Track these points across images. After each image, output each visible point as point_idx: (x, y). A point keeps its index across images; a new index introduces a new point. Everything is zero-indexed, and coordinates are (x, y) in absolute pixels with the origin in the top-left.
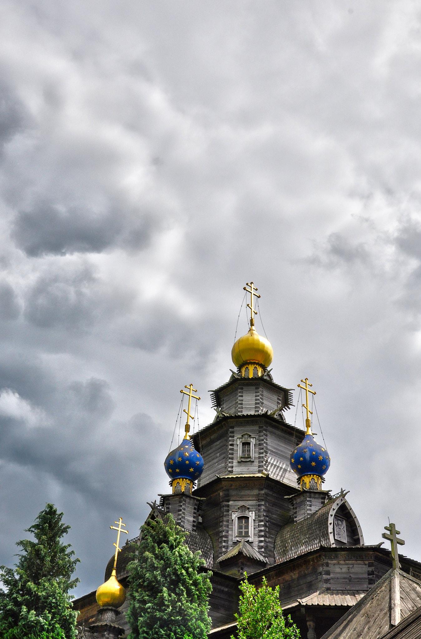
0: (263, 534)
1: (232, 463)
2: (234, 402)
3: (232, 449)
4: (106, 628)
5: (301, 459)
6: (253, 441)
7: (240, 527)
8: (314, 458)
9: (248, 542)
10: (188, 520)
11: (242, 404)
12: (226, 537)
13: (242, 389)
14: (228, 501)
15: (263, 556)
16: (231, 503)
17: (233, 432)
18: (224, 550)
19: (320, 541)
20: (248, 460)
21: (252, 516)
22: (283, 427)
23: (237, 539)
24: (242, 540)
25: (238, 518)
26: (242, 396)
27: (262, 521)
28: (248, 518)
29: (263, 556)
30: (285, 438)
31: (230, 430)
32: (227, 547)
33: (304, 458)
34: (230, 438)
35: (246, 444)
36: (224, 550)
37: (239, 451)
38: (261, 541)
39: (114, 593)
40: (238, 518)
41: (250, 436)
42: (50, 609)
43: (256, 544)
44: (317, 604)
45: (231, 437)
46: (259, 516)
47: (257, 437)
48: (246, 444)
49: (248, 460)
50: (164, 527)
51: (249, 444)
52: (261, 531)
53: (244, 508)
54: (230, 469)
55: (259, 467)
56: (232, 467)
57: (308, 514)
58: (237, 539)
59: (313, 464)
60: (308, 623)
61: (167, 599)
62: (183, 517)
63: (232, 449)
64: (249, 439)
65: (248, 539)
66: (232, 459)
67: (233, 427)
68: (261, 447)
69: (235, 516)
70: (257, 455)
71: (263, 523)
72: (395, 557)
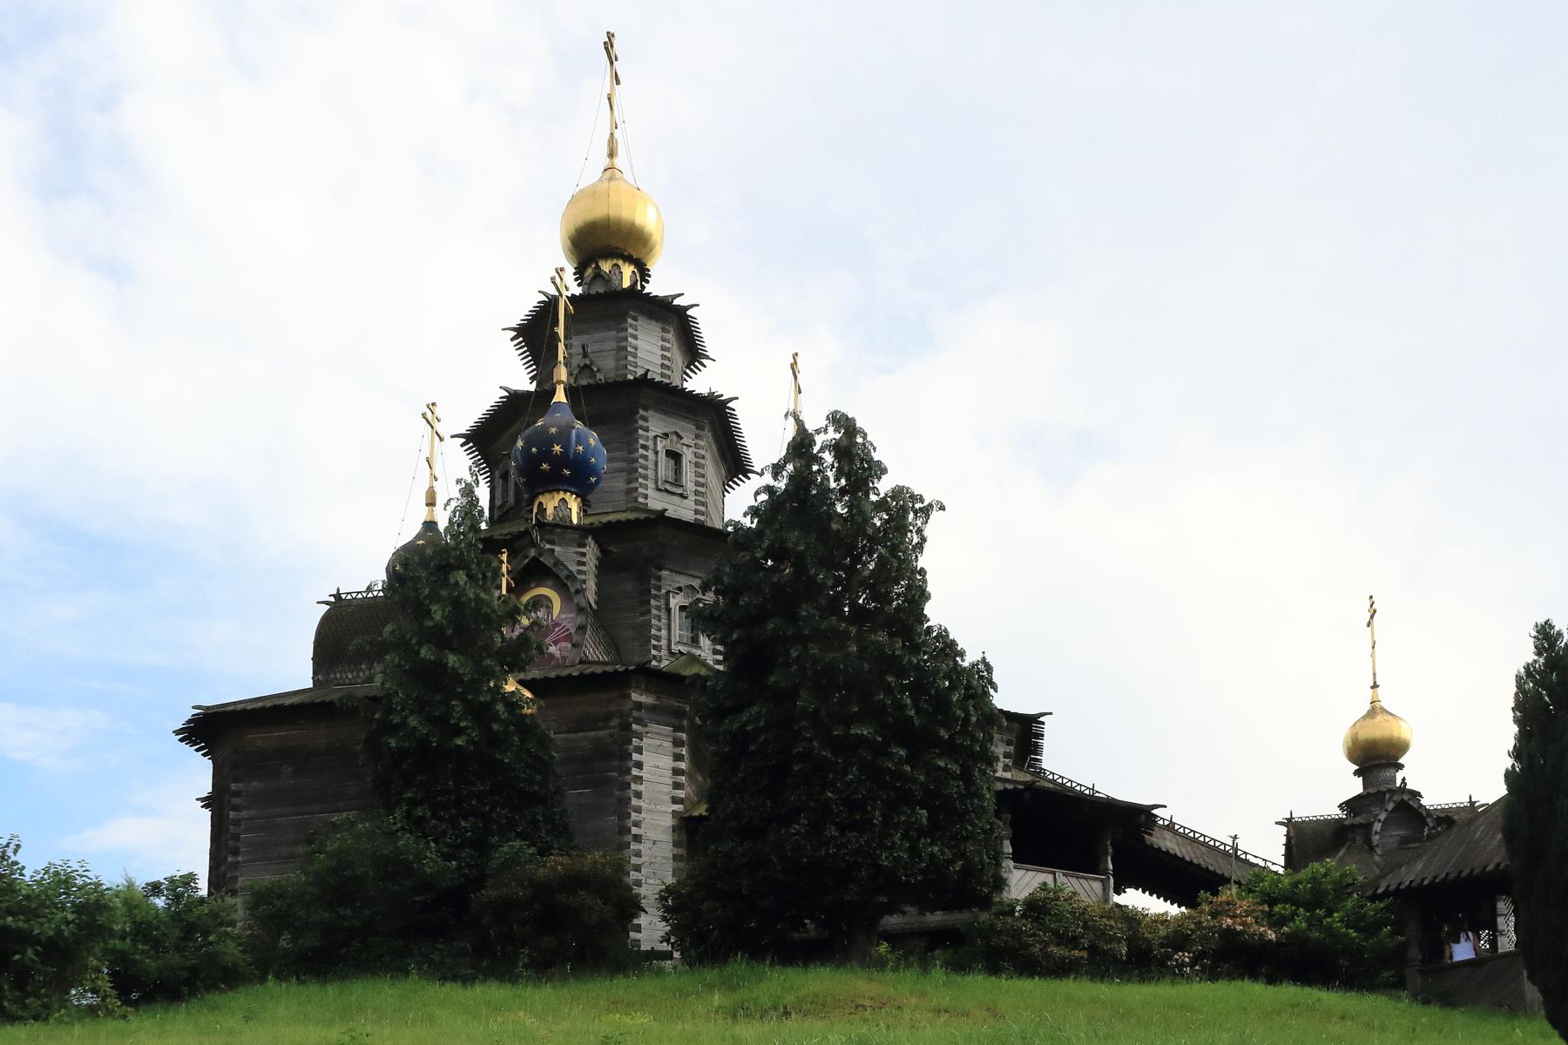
16: (665, 573)
23: (681, 648)
31: (642, 412)
49: (680, 491)
58: (681, 648)
67: (646, 410)
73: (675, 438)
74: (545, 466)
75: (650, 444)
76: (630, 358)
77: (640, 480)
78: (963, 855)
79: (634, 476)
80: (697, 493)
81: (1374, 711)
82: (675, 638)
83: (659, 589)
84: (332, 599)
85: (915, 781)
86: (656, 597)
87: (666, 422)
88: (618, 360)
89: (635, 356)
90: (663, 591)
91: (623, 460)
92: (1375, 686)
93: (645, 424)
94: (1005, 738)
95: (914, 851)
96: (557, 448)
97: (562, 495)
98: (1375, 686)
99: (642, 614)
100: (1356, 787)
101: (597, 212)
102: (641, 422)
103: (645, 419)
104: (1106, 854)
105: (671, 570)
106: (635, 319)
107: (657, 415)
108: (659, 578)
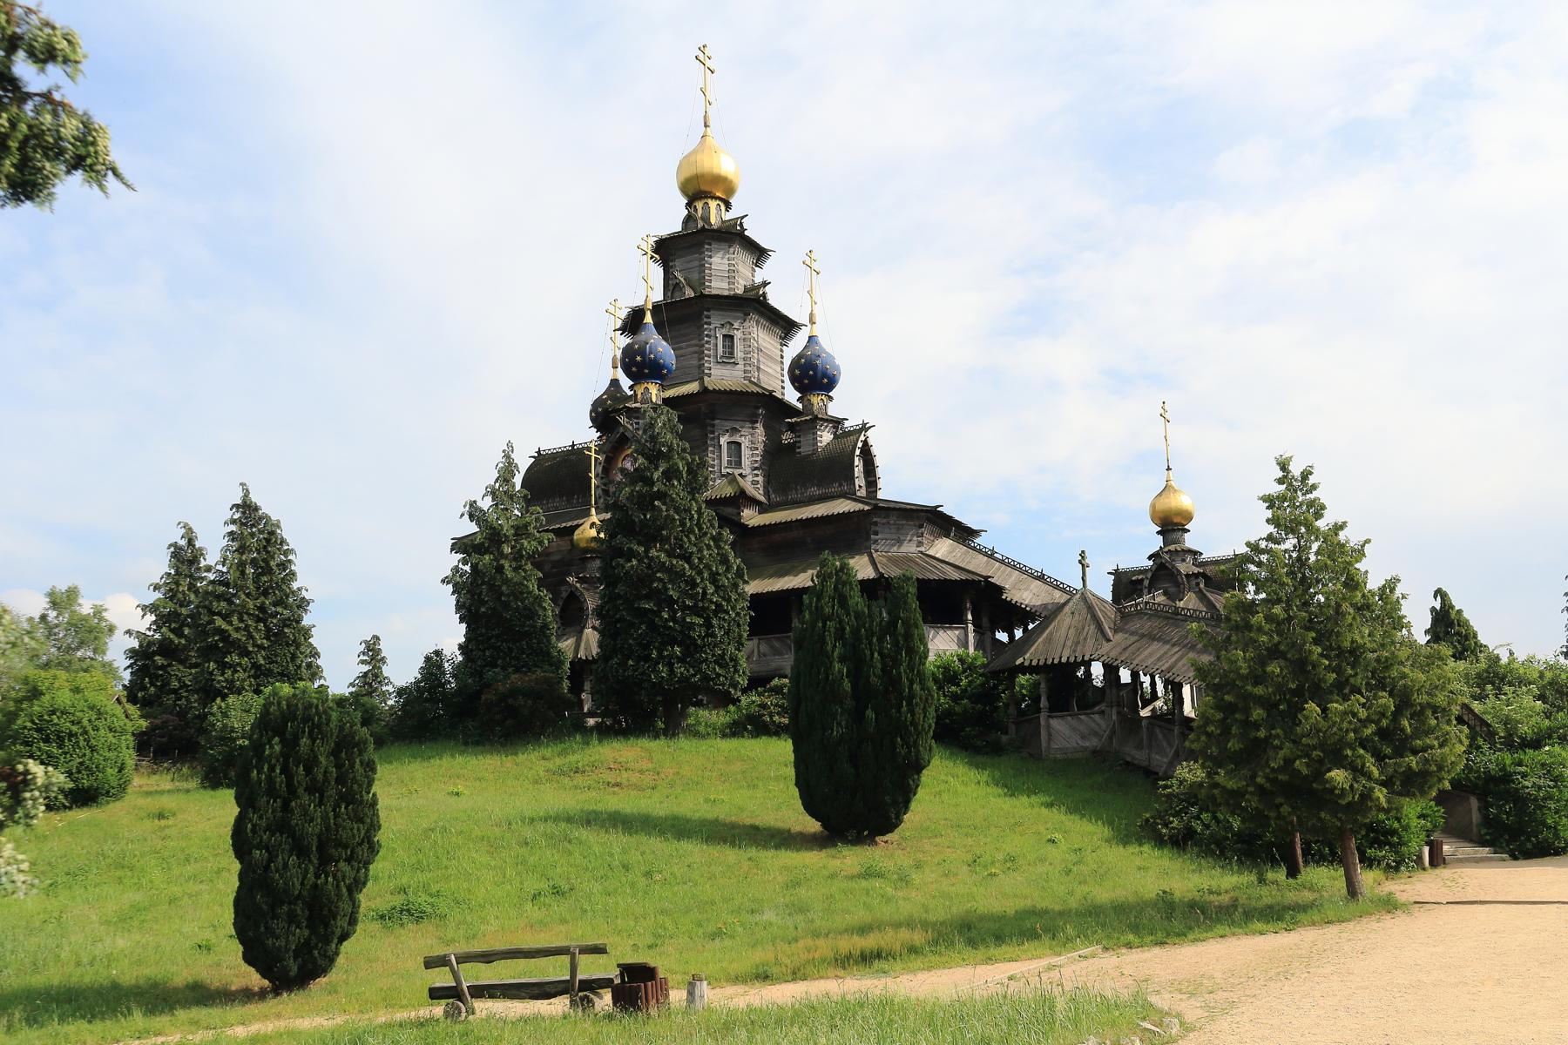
2: (697, 263)
4: (1298, 603)
5: (811, 372)
6: (738, 335)
8: (825, 375)
14: (713, 419)
15: (20, 7)
16: (717, 422)
19: (841, 485)
22: (772, 315)
23: (728, 470)
25: (728, 443)
28: (740, 444)
29: (20, 7)
31: (706, 313)
33: (815, 373)
34: (706, 326)
39: (421, 743)
40: (728, 443)
44: (1142, 680)
45: (706, 323)
48: (729, 338)
49: (732, 361)
53: (735, 431)
58: (728, 470)
60: (879, 592)
67: (708, 310)
73: (728, 326)
74: (634, 369)
75: (712, 333)
76: (707, 271)
77: (706, 358)
78: (699, 671)
79: (702, 356)
80: (744, 359)
81: (1167, 488)
82: (725, 463)
83: (713, 432)
84: (536, 455)
85: (676, 630)
86: (713, 439)
87: (723, 315)
88: (700, 273)
89: (710, 269)
90: (717, 434)
91: (696, 345)
92: (1169, 469)
93: (709, 320)
94: (917, 523)
95: (672, 671)
96: (638, 358)
97: (646, 385)
98: (1169, 469)
99: (704, 451)
100: (1157, 543)
101: (687, 174)
102: (705, 320)
103: (708, 317)
104: (967, 610)
105: (721, 419)
106: (710, 245)
107: (716, 313)
108: (713, 426)
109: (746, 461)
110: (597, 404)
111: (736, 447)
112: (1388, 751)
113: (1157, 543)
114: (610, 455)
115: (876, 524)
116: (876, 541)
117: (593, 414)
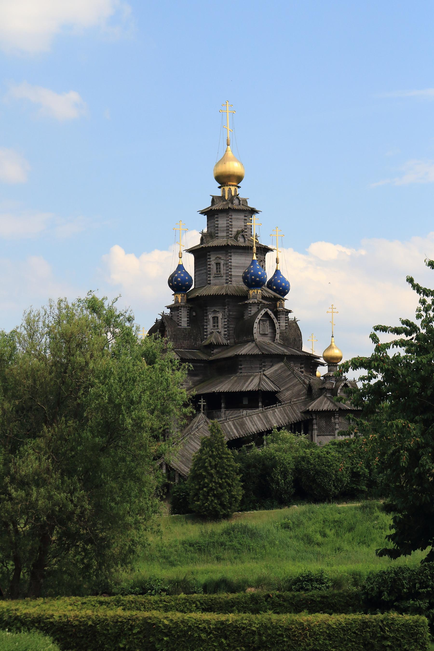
0: (226, 326)
1: (210, 277)
3: (210, 268)
6: (222, 262)
7: (214, 323)
9: (218, 332)
10: (184, 321)
11: (217, 227)
12: (206, 329)
13: (217, 215)
16: (208, 308)
17: (209, 255)
18: (205, 337)
20: (220, 275)
21: (220, 316)
24: (215, 331)
25: (213, 317)
26: (217, 221)
27: (225, 319)
30: (245, 253)
31: (208, 254)
32: (207, 335)
35: (218, 264)
36: (205, 337)
37: (213, 267)
38: (225, 331)
39: (206, 522)
40: (213, 317)
41: (220, 258)
42: (195, 412)
43: (223, 333)
46: (224, 316)
47: (225, 259)
48: (218, 264)
49: (220, 275)
50: (139, 500)
51: (219, 264)
52: (225, 325)
53: (215, 312)
54: (209, 282)
55: (227, 279)
56: (210, 280)
57: (249, 316)
59: (253, 283)
61: (110, 470)
62: (181, 320)
63: (210, 268)
64: (219, 260)
65: (218, 330)
66: (210, 274)
67: (209, 252)
68: (228, 265)
69: (210, 317)
70: (225, 272)
71: (226, 320)
72: (266, 350)
91: (204, 269)
92: (332, 337)
107: (212, 253)
109: (220, 324)
110: (172, 276)
111: (215, 319)
112: (27, 453)
113: (374, 346)
114: (161, 329)
115: (241, 361)
116: (241, 369)
117: (171, 284)
